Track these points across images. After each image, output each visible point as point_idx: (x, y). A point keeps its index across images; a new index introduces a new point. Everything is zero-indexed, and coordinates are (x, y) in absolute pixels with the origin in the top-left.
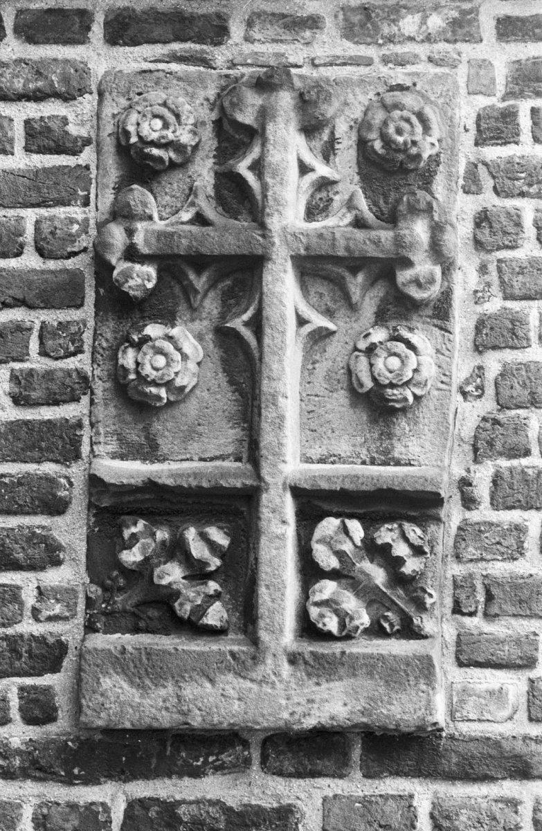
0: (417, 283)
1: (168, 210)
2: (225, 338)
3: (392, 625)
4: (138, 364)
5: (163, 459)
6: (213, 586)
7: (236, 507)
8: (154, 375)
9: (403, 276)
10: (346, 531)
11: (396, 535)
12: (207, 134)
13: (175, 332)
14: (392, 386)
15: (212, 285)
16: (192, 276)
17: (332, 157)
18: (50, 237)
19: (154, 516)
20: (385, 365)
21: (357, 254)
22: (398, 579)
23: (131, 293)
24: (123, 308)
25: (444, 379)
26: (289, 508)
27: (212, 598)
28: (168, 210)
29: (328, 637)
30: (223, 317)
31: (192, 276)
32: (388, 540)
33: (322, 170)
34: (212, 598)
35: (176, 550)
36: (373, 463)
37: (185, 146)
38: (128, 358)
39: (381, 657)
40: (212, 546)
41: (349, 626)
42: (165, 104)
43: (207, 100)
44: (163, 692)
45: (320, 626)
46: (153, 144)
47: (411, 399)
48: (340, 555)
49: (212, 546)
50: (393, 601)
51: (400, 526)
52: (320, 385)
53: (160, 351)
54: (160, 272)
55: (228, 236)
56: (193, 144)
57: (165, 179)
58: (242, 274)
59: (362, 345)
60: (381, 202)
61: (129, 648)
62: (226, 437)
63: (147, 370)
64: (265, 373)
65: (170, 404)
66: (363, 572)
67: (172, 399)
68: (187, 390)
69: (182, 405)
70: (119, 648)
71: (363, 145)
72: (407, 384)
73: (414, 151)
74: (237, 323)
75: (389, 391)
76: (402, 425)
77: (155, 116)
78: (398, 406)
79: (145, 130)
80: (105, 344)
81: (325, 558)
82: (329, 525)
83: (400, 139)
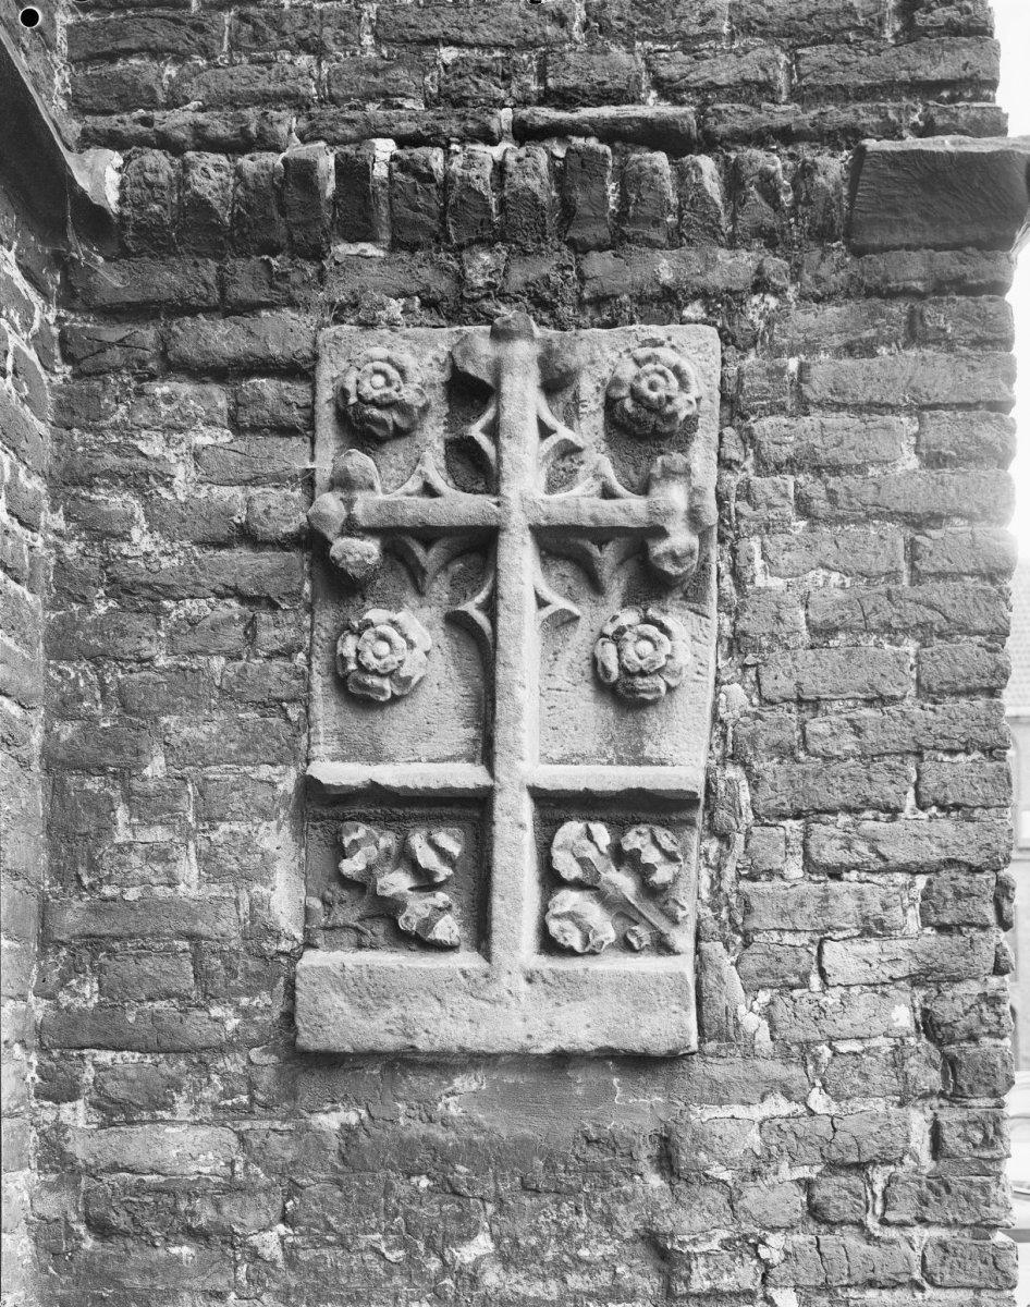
0: (675, 558)
1: (393, 484)
2: (457, 623)
3: (640, 940)
4: (358, 652)
5: (391, 759)
6: (441, 898)
7: (472, 811)
8: (375, 664)
9: (659, 548)
10: (589, 836)
11: (647, 839)
12: (436, 397)
13: (400, 617)
14: (643, 673)
15: (444, 568)
16: (419, 551)
17: (576, 423)
18: (263, 517)
19: (385, 822)
20: (637, 652)
21: (604, 524)
22: (651, 891)
23: (350, 571)
24: (343, 587)
25: (701, 669)
26: (527, 810)
27: (442, 910)
28: (393, 484)
29: (571, 952)
30: (454, 601)
31: (419, 551)
32: (638, 846)
33: (564, 432)
34: (442, 910)
35: (405, 858)
36: (621, 762)
37: (410, 407)
38: (349, 646)
39: (629, 976)
40: (443, 854)
41: (593, 941)
42: (389, 360)
43: (437, 359)
44: (387, 1014)
45: (561, 940)
46: (374, 403)
47: (663, 689)
48: (583, 862)
49: (443, 854)
50: (641, 914)
51: (651, 831)
52: (562, 678)
53: (383, 638)
54: (385, 551)
55: (461, 506)
56: (420, 404)
57: (389, 448)
58: (477, 548)
59: (610, 630)
60: (631, 473)
61: (349, 965)
62: (459, 734)
63: (368, 658)
64: (501, 657)
65: (395, 699)
66: (610, 883)
67: (397, 693)
68: (414, 681)
69: (409, 701)
70: (339, 965)
71: (610, 404)
72: (659, 671)
73: (669, 409)
74: (471, 607)
75: (639, 680)
76: (652, 718)
77: (377, 372)
78: (649, 697)
79: (366, 388)
80: (324, 635)
81: (567, 867)
82: (571, 830)
83: (654, 395)
